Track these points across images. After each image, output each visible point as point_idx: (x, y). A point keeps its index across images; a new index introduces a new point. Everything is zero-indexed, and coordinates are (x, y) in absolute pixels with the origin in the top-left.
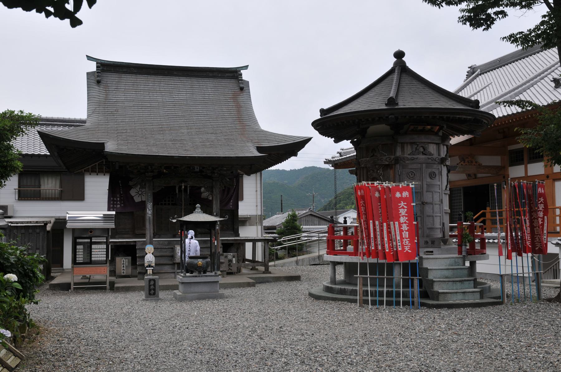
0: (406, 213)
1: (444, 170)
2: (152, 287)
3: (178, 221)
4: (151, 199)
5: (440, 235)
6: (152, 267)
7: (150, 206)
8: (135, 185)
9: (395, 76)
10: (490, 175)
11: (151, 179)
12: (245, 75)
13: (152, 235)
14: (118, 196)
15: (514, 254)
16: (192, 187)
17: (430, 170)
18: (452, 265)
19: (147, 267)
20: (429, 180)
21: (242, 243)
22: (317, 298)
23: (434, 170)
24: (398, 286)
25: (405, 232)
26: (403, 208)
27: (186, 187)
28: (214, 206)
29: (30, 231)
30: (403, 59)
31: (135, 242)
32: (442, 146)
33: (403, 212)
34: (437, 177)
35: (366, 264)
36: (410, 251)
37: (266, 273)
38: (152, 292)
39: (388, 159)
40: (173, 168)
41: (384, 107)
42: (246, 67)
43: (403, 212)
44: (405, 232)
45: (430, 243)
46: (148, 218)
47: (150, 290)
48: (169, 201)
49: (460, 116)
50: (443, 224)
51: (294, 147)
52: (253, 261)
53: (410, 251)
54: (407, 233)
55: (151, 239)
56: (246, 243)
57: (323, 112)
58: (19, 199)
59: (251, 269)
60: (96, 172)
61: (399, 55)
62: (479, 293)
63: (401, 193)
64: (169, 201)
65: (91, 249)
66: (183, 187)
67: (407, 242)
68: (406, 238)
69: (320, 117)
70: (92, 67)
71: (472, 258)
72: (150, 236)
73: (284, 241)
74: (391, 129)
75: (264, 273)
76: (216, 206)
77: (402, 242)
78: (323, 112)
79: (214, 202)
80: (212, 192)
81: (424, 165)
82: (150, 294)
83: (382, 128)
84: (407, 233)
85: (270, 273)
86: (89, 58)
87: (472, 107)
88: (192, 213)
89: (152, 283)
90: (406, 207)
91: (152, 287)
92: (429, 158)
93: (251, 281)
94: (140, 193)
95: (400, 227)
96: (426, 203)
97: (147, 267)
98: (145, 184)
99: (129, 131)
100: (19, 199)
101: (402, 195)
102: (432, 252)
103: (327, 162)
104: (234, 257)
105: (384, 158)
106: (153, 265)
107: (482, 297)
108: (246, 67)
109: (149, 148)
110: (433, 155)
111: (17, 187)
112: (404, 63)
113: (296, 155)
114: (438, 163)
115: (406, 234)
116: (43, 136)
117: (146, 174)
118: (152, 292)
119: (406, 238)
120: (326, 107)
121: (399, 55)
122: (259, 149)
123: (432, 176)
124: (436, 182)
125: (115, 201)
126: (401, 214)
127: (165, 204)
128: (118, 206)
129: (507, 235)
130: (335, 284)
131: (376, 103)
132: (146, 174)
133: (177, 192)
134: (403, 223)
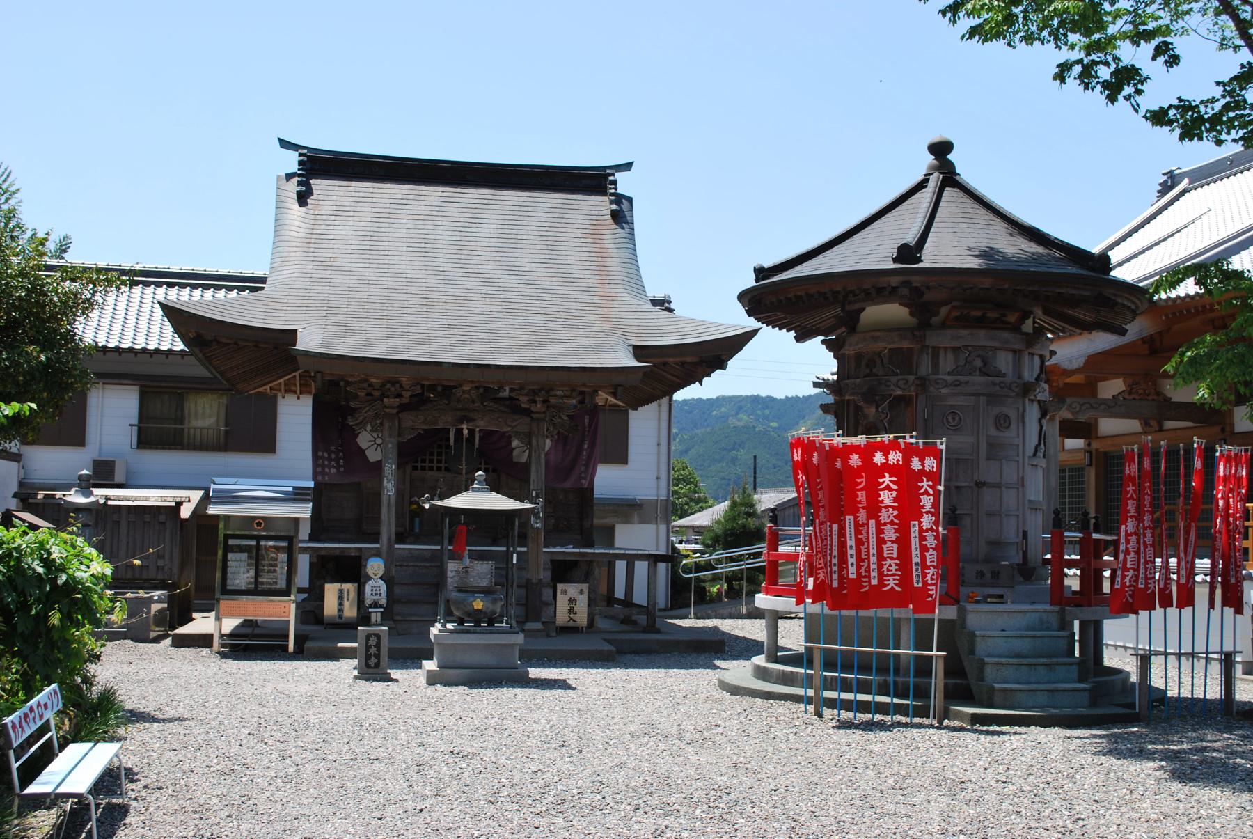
0: (895, 500)
1: (1033, 413)
3: (432, 506)
4: (393, 456)
5: (1018, 559)
6: (381, 606)
7: (390, 469)
8: (362, 424)
9: (927, 195)
10: (1189, 424)
11: (395, 411)
13: (393, 537)
14: (333, 448)
16: (487, 434)
17: (996, 410)
18: (1033, 629)
19: (371, 606)
20: (993, 432)
21: (610, 562)
22: (735, 690)
23: (1006, 410)
24: (907, 674)
25: (889, 544)
26: (888, 488)
27: (471, 432)
28: (533, 476)
29: (147, 517)
30: (949, 157)
31: (360, 549)
32: (1026, 358)
33: (927, 502)
34: (1014, 426)
35: (887, 619)
36: (898, 589)
37: (649, 632)
38: (373, 661)
39: (901, 383)
40: (439, 389)
41: (891, 265)
42: (628, 166)
43: (927, 502)
44: (889, 544)
45: (988, 575)
46: (384, 499)
47: (368, 657)
48: (439, 461)
49: (1063, 291)
50: (1025, 533)
51: (715, 354)
52: (627, 603)
53: (898, 589)
54: (895, 546)
55: (390, 546)
56: (637, 563)
57: (761, 273)
58: (138, 447)
59: (622, 622)
60: (295, 392)
61: (941, 149)
62: (1087, 694)
63: (886, 455)
64: (439, 461)
65: (776, 627)
66: (465, 432)
67: (894, 567)
68: (892, 559)
69: (754, 284)
70: (291, 161)
71: (1089, 613)
72: (389, 539)
73: (719, 561)
74: (912, 314)
75: (645, 631)
76: (537, 477)
77: (880, 566)
78: (761, 273)
79: (533, 469)
80: (530, 443)
81: (983, 399)
82: (368, 666)
83: (893, 311)
84: (895, 546)
85: (658, 631)
86: (284, 144)
87: (1093, 270)
88: (467, 489)
89: (373, 641)
90: (894, 487)
91: (373, 651)
92: (994, 384)
93: (607, 647)
94: (379, 441)
95: (879, 531)
96: (984, 484)
97: (371, 606)
98: (382, 424)
99: (353, 305)
100: (138, 447)
101: (887, 459)
102: (1001, 596)
103: (816, 385)
104: (581, 592)
105: (894, 379)
106: (384, 602)
107: (1094, 703)
108: (628, 166)
109: (391, 342)
110: (1004, 375)
111: (135, 421)
112: (951, 164)
113: (723, 367)
114: (1017, 395)
115: (931, 557)
116: (171, 312)
117: (386, 400)
118: (373, 661)
119: (892, 559)
120: (767, 265)
121: (941, 149)
122: (639, 351)
123: (1002, 422)
124: (1011, 434)
125: (338, 463)
126: (882, 502)
127: (431, 469)
128: (333, 471)
129: (1214, 565)
130: (776, 662)
131: (871, 253)
132: (386, 400)
133: (452, 443)
134: (885, 524)
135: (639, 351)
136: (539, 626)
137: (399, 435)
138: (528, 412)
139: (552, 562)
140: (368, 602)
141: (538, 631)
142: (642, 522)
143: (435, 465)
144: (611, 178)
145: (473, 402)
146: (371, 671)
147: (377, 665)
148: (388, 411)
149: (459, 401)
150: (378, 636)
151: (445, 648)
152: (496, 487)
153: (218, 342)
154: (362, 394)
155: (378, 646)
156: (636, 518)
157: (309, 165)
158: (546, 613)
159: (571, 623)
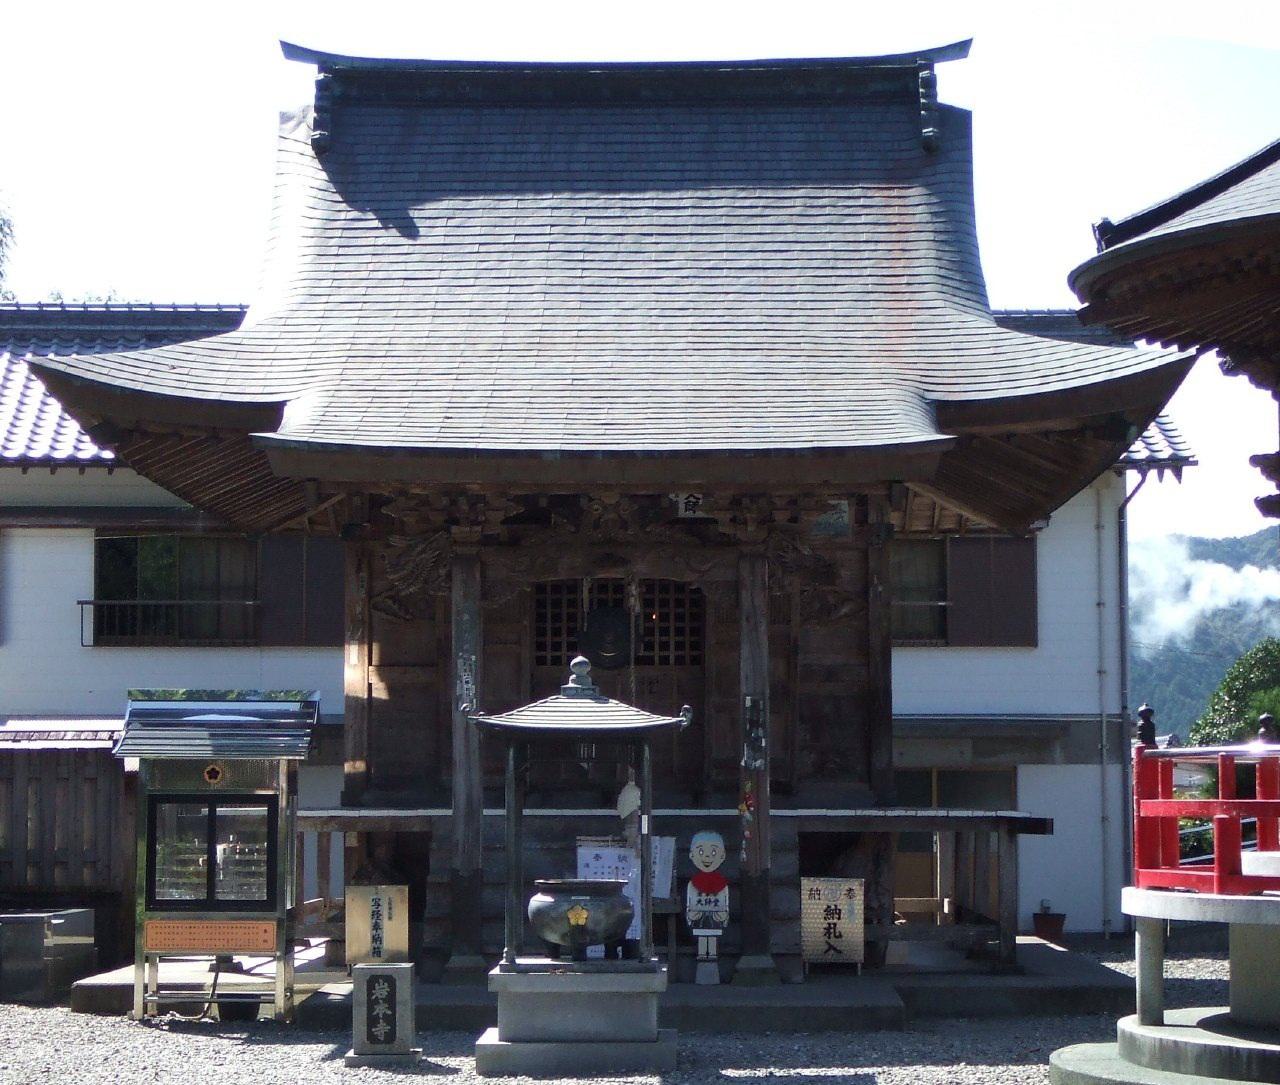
2: (381, 1009)
6: (717, 926)
12: (952, 85)
13: (478, 793)
15: (183, 836)
19: (696, 924)
38: (381, 1029)
42: (960, 49)
48: (664, 646)
55: (472, 814)
57: (1107, 232)
69: (1094, 254)
72: (469, 797)
78: (1107, 232)
86: (292, 51)
89: (381, 991)
91: (381, 1009)
97: (696, 924)
98: (449, 576)
106: (725, 924)
108: (960, 49)
117: (454, 529)
118: (381, 1029)
120: (1116, 220)
122: (943, 413)
135: (943, 413)
136: (765, 961)
137: (484, 596)
138: (727, 542)
139: (804, 837)
140: (691, 916)
141: (764, 971)
142: (1070, 760)
143: (657, 653)
144: (923, 74)
145: (624, 525)
146: (379, 1047)
147: (391, 1037)
148: (459, 549)
149: (596, 526)
150: (390, 980)
151: (530, 1001)
152: (603, 688)
153: (145, 434)
154: (410, 519)
155: (391, 1000)
156: (1058, 753)
157: (337, 90)
158: (778, 938)
159: (831, 957)
